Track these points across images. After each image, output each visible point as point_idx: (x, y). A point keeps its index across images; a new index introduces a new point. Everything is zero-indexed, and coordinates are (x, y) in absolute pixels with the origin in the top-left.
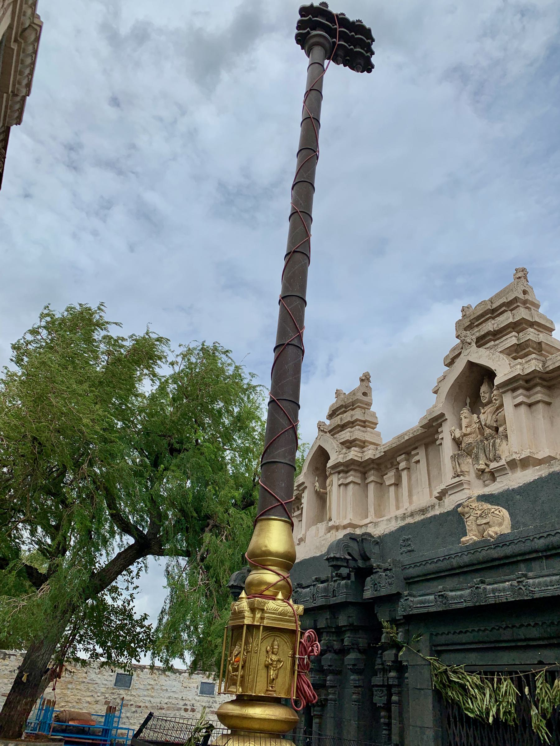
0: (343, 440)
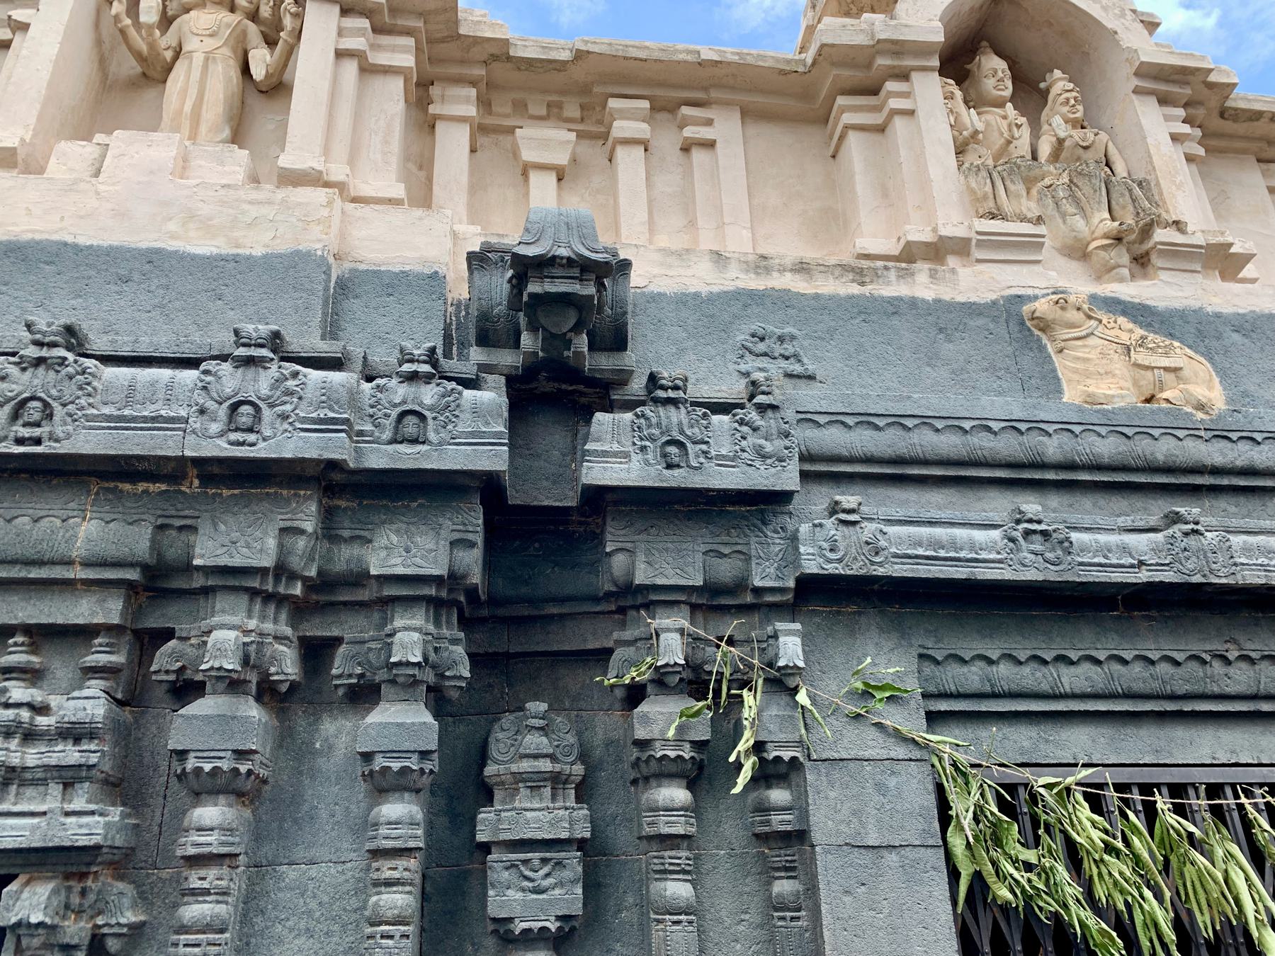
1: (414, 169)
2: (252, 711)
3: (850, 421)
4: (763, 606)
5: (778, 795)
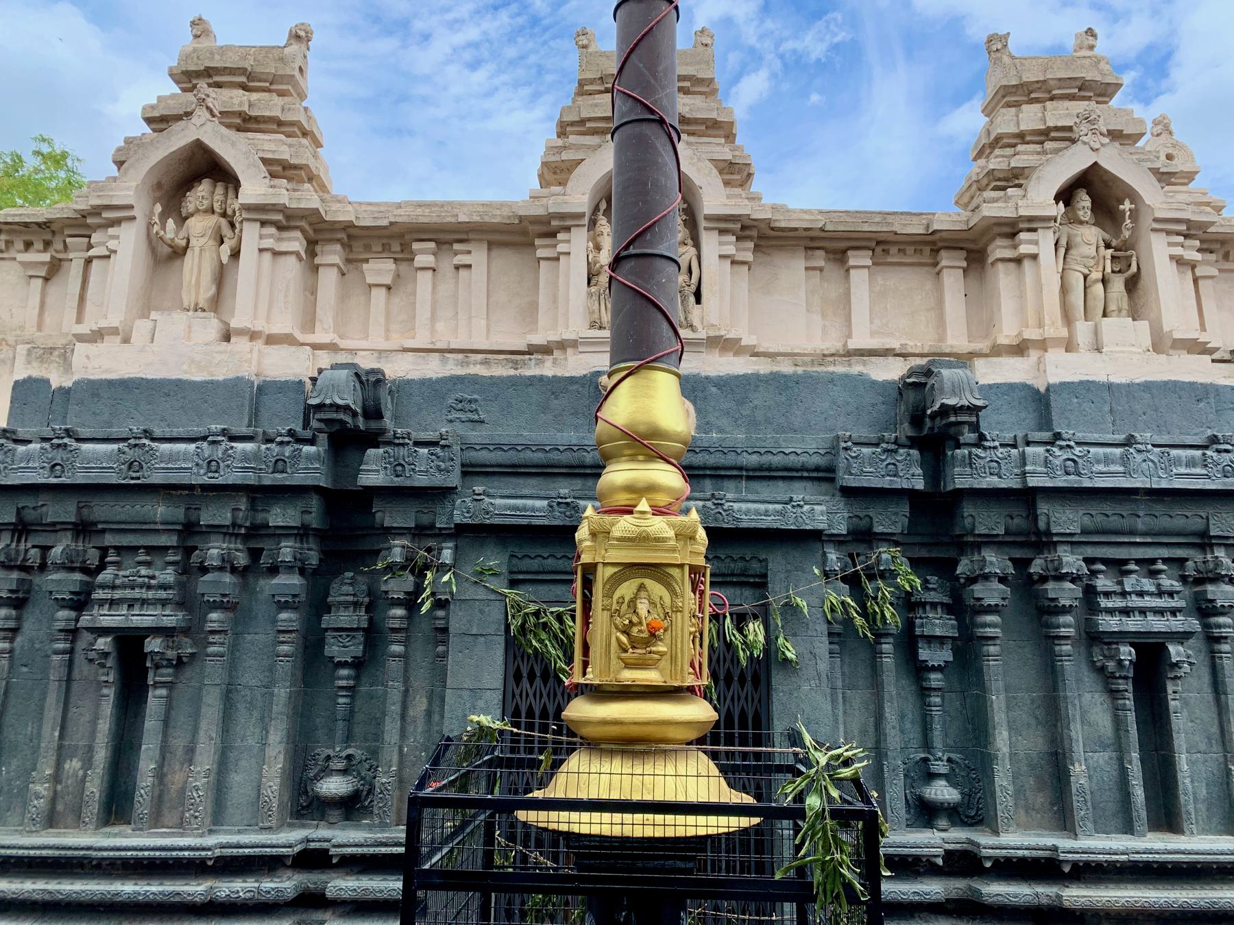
0: (269, 156)
1: (307, 293)
2: (227, 578)
3: (491, 448)
4: (443, 535)
5: (441, 613)
